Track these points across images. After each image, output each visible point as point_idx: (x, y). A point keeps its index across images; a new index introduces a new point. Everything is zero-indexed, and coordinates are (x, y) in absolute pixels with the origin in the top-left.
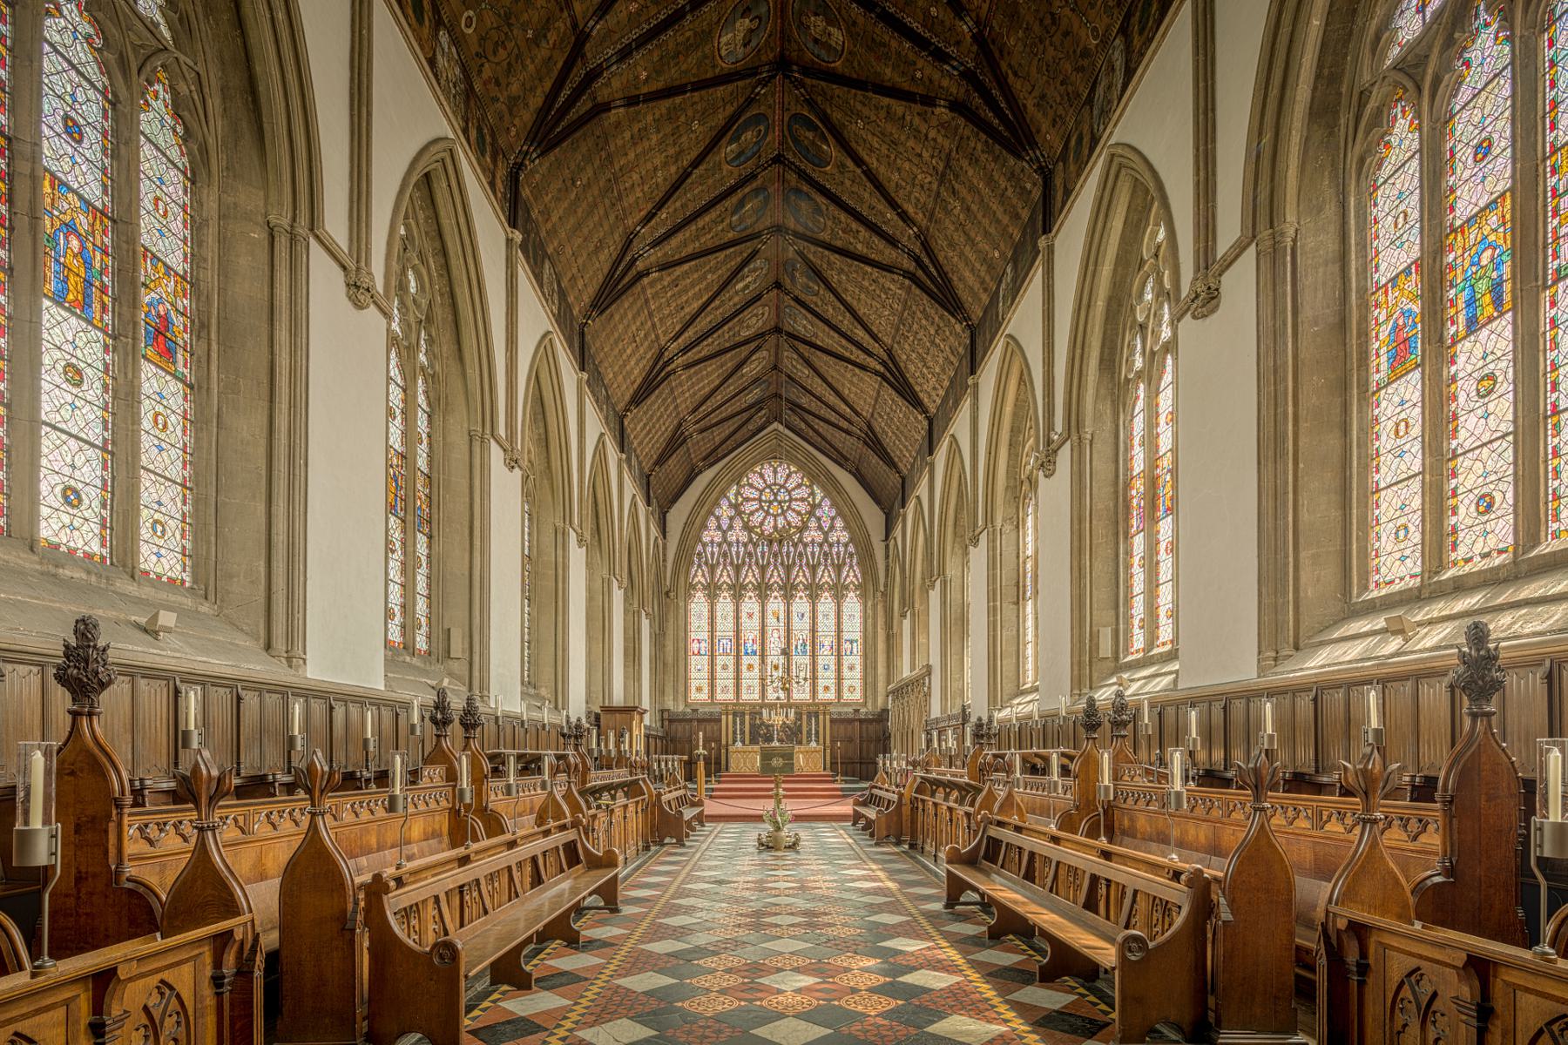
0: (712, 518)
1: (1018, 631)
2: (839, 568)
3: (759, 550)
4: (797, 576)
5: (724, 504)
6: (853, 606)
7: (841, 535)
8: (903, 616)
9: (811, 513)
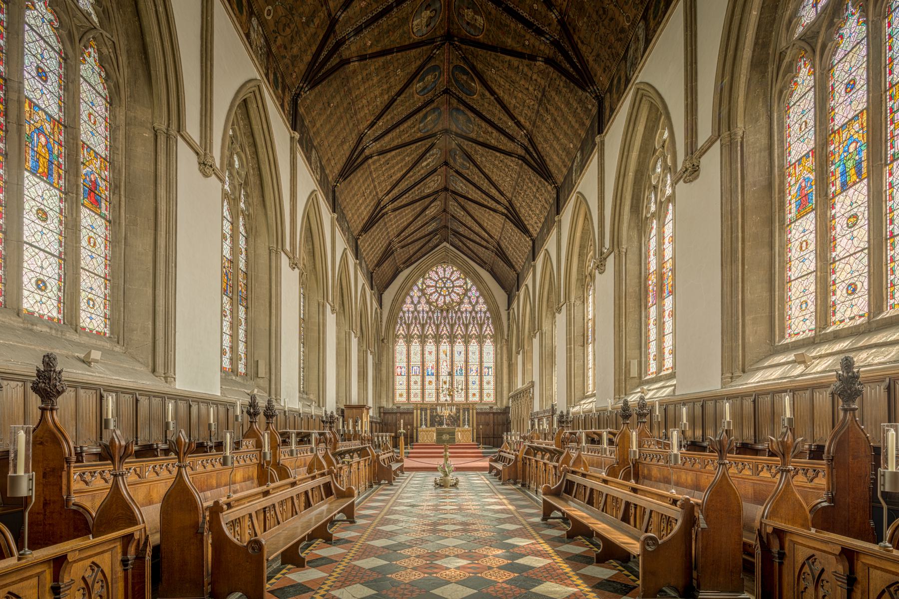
0: (408, 297)
1: (584, 362)
2: (481, 326)
3: (435, 315)
4: (457, 330)
5: (415, 289)
6: (489, 347)
7: (482, 307)
8: (518, 353)
9: (465, 294)
